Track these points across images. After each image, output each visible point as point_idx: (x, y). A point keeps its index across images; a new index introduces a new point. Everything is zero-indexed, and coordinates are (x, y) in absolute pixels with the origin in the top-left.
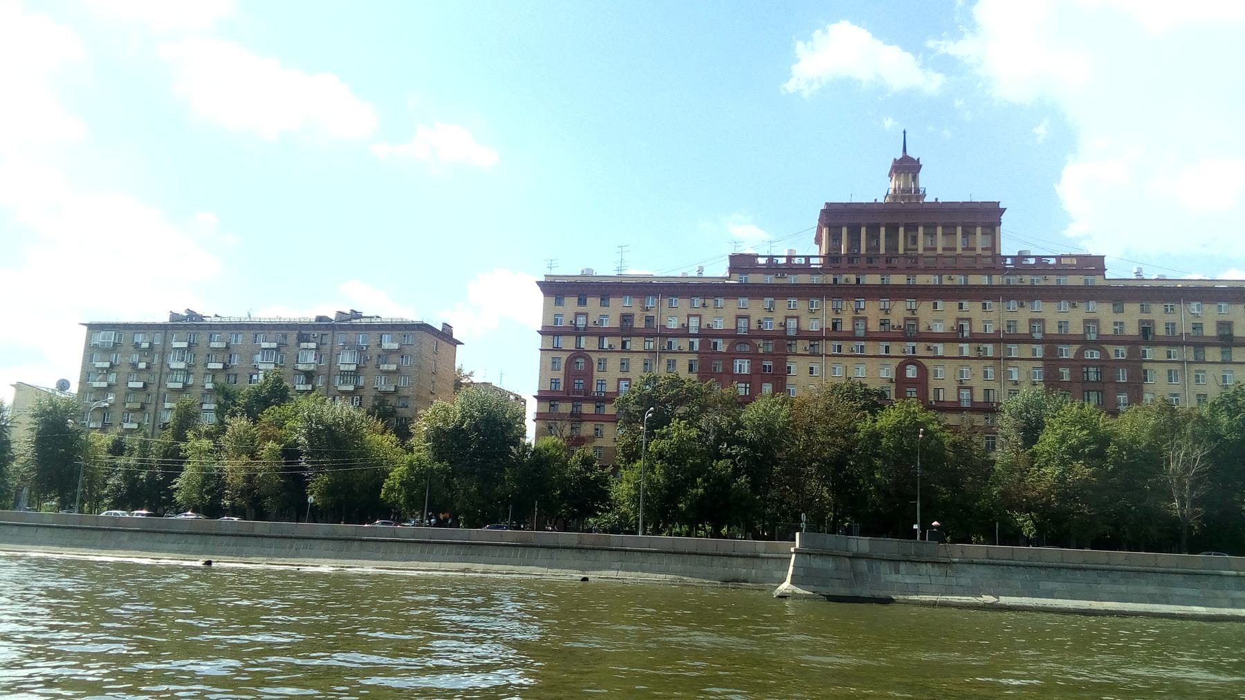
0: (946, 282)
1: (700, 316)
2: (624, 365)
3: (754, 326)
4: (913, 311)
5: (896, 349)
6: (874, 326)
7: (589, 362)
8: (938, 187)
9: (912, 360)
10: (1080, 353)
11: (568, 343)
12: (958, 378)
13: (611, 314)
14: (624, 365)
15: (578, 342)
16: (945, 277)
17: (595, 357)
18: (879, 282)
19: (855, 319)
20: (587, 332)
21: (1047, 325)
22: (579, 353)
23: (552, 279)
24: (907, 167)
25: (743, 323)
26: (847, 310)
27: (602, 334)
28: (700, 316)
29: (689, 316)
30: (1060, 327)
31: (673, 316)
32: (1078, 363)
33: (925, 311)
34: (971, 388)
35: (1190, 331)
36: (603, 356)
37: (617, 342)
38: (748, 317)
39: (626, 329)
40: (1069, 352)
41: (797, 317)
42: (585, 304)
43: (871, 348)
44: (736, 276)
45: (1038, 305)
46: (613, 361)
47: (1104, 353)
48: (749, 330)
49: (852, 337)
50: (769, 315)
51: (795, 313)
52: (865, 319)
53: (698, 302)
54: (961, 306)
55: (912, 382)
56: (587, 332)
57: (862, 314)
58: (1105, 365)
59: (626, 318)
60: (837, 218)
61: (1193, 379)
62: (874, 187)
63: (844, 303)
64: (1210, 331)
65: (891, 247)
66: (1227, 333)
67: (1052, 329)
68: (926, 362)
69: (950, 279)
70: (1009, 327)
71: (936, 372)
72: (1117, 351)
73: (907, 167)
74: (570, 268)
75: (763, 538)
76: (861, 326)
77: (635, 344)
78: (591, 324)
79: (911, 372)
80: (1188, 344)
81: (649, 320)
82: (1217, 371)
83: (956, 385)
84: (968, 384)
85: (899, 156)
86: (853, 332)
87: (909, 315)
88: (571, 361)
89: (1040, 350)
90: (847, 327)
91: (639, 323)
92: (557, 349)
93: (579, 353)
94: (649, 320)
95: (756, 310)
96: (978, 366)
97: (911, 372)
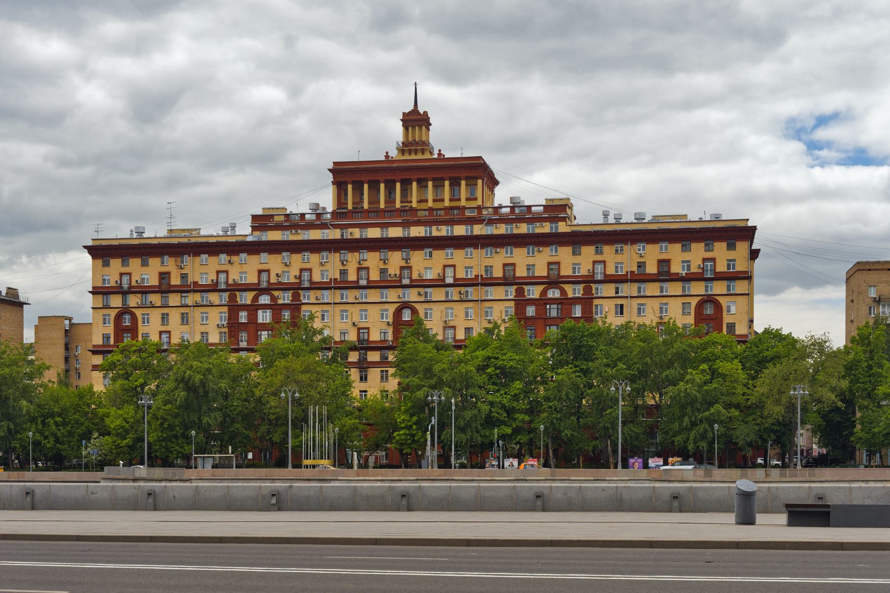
0: (435, 233)
1: (227, 272)
2: (165, 318)
3: (273, 280)
4: (407, 260)
5: (393, 295)
6: (375, 276)
7: (134, 318)
8: (446, 140)
9: (405, 305)
10: (544, 293)
11: (116, 301)
12: (444, 319)
13: (147, 273)
14: (165, 318)
15: (124, 301)
16: (434, 228)
17: (139, 313)
18: (423, 234)
19: (359, 269)
20: (131, 291)
21: (517, 269)
22: (710, 299)
23: (98, 243)
24: (415, 120)
25: (599, 268)
26: (353, 259)
27: (144, 291)
28: (227, 272)
29: (218, 272)
30: (528, 269)
31: (204, 270)
32: (542, 302)
33: (418, 258)
34: (454, 327)
35: (635, 269)
36: (145, 311)
37: (156, 299)
38: (268, 271)
39: (164, 288)
40: (534, 292)
41: (454, 266)
42: (602, 253)
43: (373, 295)
44: (257, 233)
45: (264, 256)
46: (155, 316)
47: (563, 292)
48: (605, 275)
49: (356, 286)
50: (286, 269)
51: (308, 266)
52: (367, 269)
53: (223, 257)
54: (163, 263)
55: (408, 324)
56: (131, 291)
57: (365, 264)
58: (565, 303)
59: (164, 276)
60: (345, 175)
61: (635, 310)
62: (384, 139)
63: (350, 255)
64: (652, 268)
65: (358, 201)
66: (666, 269)
67: (521, 272)
68: (416, 306)
69: (517, 227)
70: (486, 271)
71: (729, 307)
72: (574, 290)
73: (415, 120)
74: (121, 231)
75: (15, 469)
76: (222, 277)
77: (174, 299)
78: (134, 284)
79: (709, 310)
80: (632, 281)
81: (184, 277)
82: (655, 304)
83: (442, 325)
84: (452, 324)
85: (409, 108)
86: (121, 286)
87: (403, 264)
88: (700, 306)
89: (512, 291)
90: (352, 277)
91: (175, 281)
92: (106, 307)
93: (125, 310)
94: (184, 277)
95: (274, 264)
96: (460, 308)
97: (407, 316)
